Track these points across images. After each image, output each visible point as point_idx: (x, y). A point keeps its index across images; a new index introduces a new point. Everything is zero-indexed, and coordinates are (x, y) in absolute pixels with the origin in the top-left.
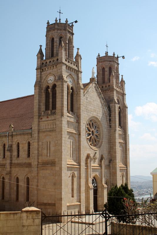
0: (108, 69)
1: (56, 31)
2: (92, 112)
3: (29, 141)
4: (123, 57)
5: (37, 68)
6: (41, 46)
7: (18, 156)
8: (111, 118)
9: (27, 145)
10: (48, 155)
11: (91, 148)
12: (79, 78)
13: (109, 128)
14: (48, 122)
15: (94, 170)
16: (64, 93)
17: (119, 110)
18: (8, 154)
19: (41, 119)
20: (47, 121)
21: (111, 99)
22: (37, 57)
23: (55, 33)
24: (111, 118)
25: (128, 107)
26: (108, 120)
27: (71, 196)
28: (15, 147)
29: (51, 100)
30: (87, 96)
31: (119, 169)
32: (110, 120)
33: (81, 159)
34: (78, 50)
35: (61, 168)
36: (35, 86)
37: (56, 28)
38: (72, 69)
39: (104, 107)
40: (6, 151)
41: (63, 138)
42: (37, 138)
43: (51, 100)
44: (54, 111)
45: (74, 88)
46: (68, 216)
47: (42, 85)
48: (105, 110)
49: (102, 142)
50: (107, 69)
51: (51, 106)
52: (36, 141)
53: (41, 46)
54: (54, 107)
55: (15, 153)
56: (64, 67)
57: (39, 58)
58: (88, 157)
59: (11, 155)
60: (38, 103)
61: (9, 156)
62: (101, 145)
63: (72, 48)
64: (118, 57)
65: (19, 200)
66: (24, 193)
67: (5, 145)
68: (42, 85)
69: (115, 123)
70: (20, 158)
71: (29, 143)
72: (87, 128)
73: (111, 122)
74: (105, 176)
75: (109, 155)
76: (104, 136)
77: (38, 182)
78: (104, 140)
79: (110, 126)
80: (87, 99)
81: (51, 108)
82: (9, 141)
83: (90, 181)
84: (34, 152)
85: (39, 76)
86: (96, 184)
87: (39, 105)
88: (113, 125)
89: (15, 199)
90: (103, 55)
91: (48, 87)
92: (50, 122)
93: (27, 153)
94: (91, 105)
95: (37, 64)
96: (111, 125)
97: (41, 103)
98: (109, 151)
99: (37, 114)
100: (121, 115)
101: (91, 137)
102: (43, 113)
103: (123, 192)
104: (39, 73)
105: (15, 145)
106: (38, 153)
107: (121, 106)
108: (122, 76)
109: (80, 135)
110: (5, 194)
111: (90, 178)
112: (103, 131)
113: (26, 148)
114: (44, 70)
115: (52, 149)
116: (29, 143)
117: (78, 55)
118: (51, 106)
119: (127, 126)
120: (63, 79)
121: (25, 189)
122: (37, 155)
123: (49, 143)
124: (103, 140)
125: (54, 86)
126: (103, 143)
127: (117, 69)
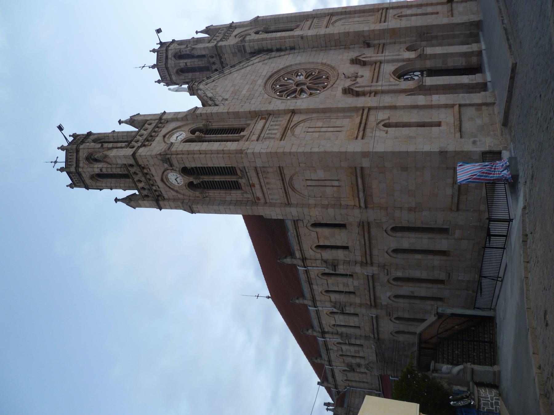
0: (182, 61)
1: (80, 170)
3: (309, 225)
4: (159, 31)
5: (157, 207)
6: (116, 200)
7: (346, 248)
8: (274, 48)
9: (319, 230)
10: (336, 183)
11: (332, 86)
12: (175, 117)
13: (296, 51)
14: (263, 184)
15: (376, 77)
16: (193, 151)
17: (260, 33)
18: (341, 269)
19: (258, 199)
20: (261, 187)
21: (236, 50)
22: (137, 208)
24: (274, 48)
25: (256, 16)
26: (278, 54)
27: (437, 128)
28: (328, 255)
29: (217, 178)
30: (220, 99)
32: (279, 50)
33: (349, 106)
34: (123, 122)
35: (365, 154)
36: (192, 212)
37: (76, 170)
38: (153, 134)
39: (251, 63)
40: (337, 272)
41: (294, 150)
42: (300, 210)
43: (217, 178)
44: (239, 173)
45: (194, 126)
47: (190, 198)
48: (257, 60)
49: (322, 63)
50: (182, 63)
52: (306, 210)
53: (116, 200)
54: (231, 171)
55: (340, 254)
56: (142, 151)
58: (347, 91)
59: (345, 262)
62: (328, 65)
63: (114, 135)
64: (161, 43)
65: (446, 250)
66: (429, 238)
67: (324, 274)
68: (190, 196)
69: (285, 38)
70: (350, 244)
71: (315, 225)
72: (288, 96)
73: (283, 47)
74: (397, 53)
75: (354, 48)
76: (311, 60)
78: (319, 61)
79: (292, 48)
80: (226, 100)
81: (233, 178)
82: (313, 265)
83: (404, 85)
84: (330, 216)
85: (171, 203)
86: (416, 73)
88: (288, 43)
89: (444, 258)
90: (155, 74)
91: (191, 185)
92: (262, 181)
93: (336, 231)
94: (240, 90)
95: (150, 207)
96: (288, 48)
97: (227, 199)
98: (345, 48)
99: (248, 208)
100: (272, 28)
101: (309, 88)
102: (245, 195)
104: (166, 203)
105: (322, 253)
107: (254, 30)
108: (197, 32)
109: (294, 110)
110: (430, 278)
111: (398, 85)
112: (300, 64)
113: (326, 231)
114: (157, 193)
115: (321, 174)
116: (315, 225)
117: (131, 121)
119: (294, 15)
120: (165, 153)
121: (420, 236)
123: (309, 183)
124: (318, 63)
125: (185, 171)
126: (324, 61)
127: (181, 43)
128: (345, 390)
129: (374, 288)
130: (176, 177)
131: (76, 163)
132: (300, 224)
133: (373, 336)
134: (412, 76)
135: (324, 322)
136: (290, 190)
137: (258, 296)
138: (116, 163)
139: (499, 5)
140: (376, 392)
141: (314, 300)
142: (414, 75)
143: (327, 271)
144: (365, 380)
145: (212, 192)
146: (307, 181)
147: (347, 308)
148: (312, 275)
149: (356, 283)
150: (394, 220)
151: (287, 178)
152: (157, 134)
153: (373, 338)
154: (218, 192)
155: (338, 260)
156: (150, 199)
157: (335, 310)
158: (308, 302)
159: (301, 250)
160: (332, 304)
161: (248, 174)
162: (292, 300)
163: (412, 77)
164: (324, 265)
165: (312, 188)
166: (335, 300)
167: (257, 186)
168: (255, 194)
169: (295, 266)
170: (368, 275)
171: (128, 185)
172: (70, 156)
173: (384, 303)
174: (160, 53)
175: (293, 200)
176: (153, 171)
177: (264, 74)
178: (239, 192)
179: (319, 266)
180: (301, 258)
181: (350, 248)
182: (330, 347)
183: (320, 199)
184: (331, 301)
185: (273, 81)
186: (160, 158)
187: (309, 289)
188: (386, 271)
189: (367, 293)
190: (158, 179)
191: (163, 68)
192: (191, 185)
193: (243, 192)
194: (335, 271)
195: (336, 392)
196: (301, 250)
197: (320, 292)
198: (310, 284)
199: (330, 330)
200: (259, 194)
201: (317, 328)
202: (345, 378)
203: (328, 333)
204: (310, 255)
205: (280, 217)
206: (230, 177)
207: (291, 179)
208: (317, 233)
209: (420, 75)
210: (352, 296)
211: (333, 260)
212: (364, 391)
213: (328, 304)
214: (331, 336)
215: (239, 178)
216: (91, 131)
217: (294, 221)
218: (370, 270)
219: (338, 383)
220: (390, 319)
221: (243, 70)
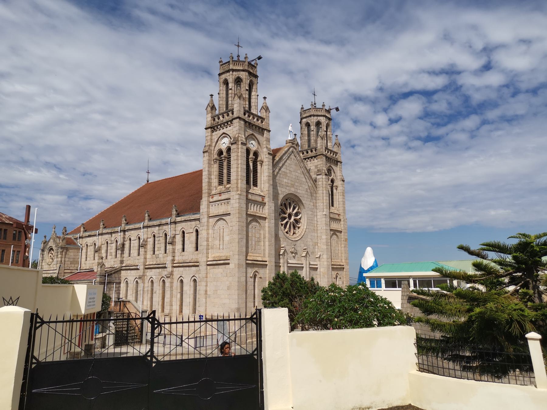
1: (231, 72)
2: (287, 188)
3: (197, 228)
7: (183, 250)
9: (194, 234)
14: (221, 202)
18: (169, 247)
23: (230, 75)
28: (179, 239)
29: (225, 171)
31: (331, 268)
37: (231, 69)
42: (206, 224)
43: (225, 171)
46: (235, 320)
48: (310, 185)
51: (220, 176)
52: (205, 228)
55: (179, 246)
57: (209, 112)
60: (207, 175)
61: (171, 250)
67: (166, 235)
72: (282, 209)
77: (206, 286)
81: (225, 182)
82: (172, 229)
87: (210, 179)
89: (178, 312)
92: (223, 201)
93: (194, 245)
97: (212, 176)
99: (207, 190)
103: (468, 360)
106: (208, 245)
118: (220, 176)
121: (191, 297)
122: (205, 248)
128: (79, 244)
129: (158, 268)
130: (226, 143)
131: (236, 70)
132: (198, 222)
133: (124, 266)
135: (133, 232)
136: (218, 218)
137: (148, 173)
140: (79, 267)
141: (147, 227)
143: (168, 237)
144: (88, 259)
145: (217, 166)
146: (222, 230)
147: (143, 249)
148: (165, 227)
149: (161, 256)
150: (200, 282)
151: (224, 218)
152: (254, 129)
153: (122, 266)
154: (217, 170)
155: (175, 245)
156: (212, 122)
157: (141, 241)
158: (146, 223)
159: (181, 222)
160: (146, 239)
161: (227, 193)
162: (147, 211)
164: (172, 236)
165: (219, 232)
166: (148, 241)
167: (220, 198)
168: (215, 195)
169: (171, 215)
170: (166, 264)
171: (221, 106)
172: (241, 64)
173: (148, 274)
174: (321, 111)
175: (211, 220)
176: (229, 128)
177: (299, 191)
178: (217, 184)
179: (171, 232)
180: (176, 221)
181: (183, 253)
182: (113, 235)
183: (212, 237)
184: (147, 238)
185: (293, 198)
186: (236, 136)
187: (155, 224)
188: (169, 276)
189: (154, 263)
190: (225, 130)
191: (311, 113)
192: (220, 153)
193: (217, 187)
194: (168, 244)
195: (76, 237)
196: (181, 222)
197: (154, 231)
198: (159, 225)
199: (127, 236)
200: (216, 198)
201: (127, 227)
202: (89, 245)
203: (124, 234)
204: (178, 227)
205: (201, 211)
206: (226, 180)
207: (224, 220)
208: (192, 233)
210: (152, 252)
211: (176, 242)
212: (79, 258)
213: (145, 237)
214: (122, 236)
215: (225, 186)
216: (258, 77)
217: (199, 219)
218: (169, 265)
219: (84, 239)
220: (136, 278)
221: (302, 176)
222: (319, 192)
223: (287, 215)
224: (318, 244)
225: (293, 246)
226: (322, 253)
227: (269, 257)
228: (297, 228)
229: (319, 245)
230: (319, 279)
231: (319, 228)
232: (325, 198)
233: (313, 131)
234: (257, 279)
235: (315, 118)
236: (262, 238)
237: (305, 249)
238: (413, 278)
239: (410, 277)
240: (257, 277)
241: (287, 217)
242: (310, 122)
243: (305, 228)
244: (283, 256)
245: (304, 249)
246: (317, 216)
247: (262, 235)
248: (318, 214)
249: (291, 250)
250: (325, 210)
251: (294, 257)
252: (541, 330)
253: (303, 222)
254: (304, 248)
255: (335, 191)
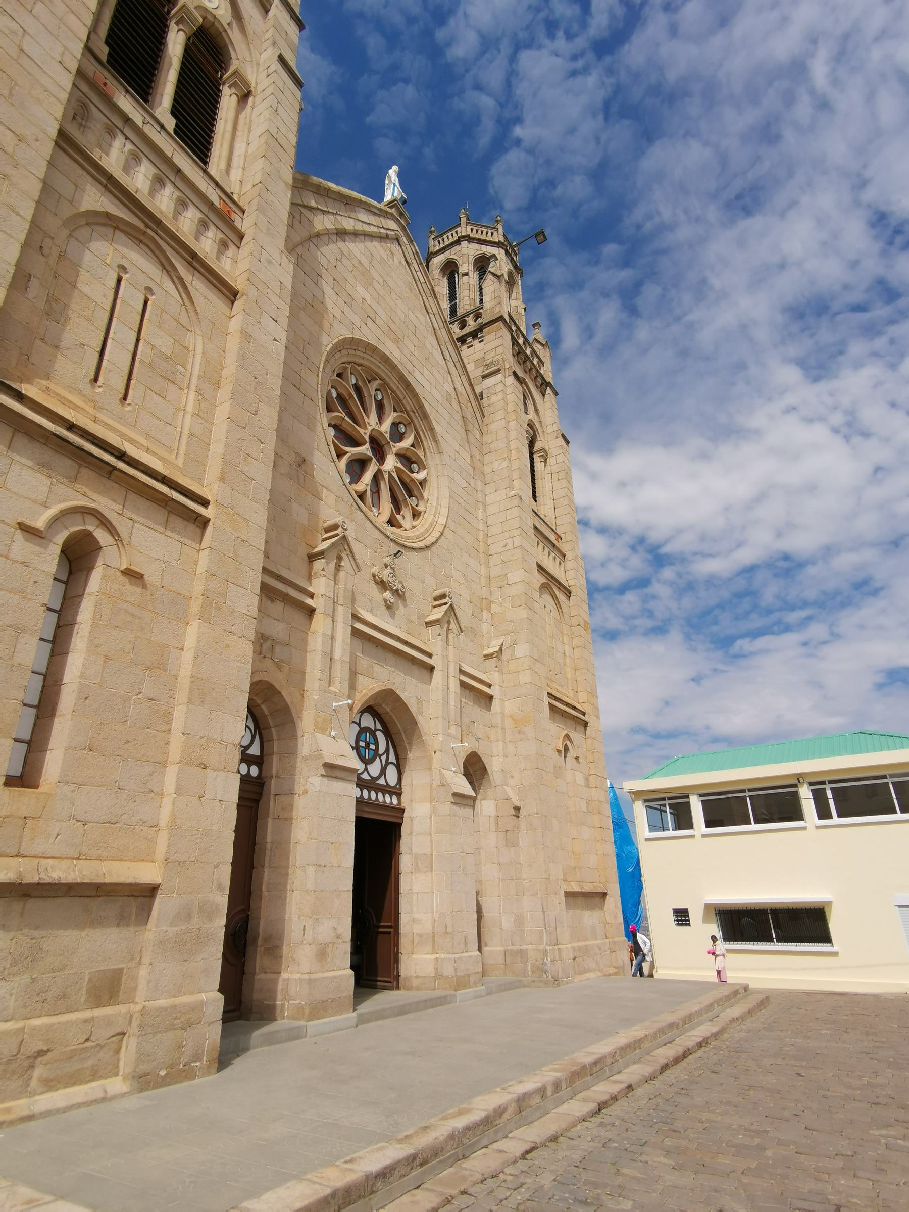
134: (384, 758)
138: (117, 231)
139: (827, 783)
142: (387, 763)
163: (380, 756)
174: (492, 234)
185: (384, 376)
209: (386, 782)
222: (493, 427)
223: (365, 450)
224: (493, 606)
225: (387, 560)
226: (507, 640)
227: (222, 479)
228: (406, 512)
229: (495, 608)
230: (501, 744)
231: (493, 549)
232: (513, 445)
233: (467, 274)
234: (95, 581)
235: (474, 246)
236: (196, 372)
237: (443, 596)
238: (810, 784)
239: (799, 778)
240: (99, 562)
241: (370, 453)
242: (456, 258)
243: (442, 520)
244: (327, 563)
245: (436, 599)
246: (485, 505)
247: (198, 358)
248: (490, 499)
249: (375, 570)
250: (516, 483)
251: (389, 607)
252: (545, 960)
253: (433, 501)
254: (437, 593)
255: (539, 465)
